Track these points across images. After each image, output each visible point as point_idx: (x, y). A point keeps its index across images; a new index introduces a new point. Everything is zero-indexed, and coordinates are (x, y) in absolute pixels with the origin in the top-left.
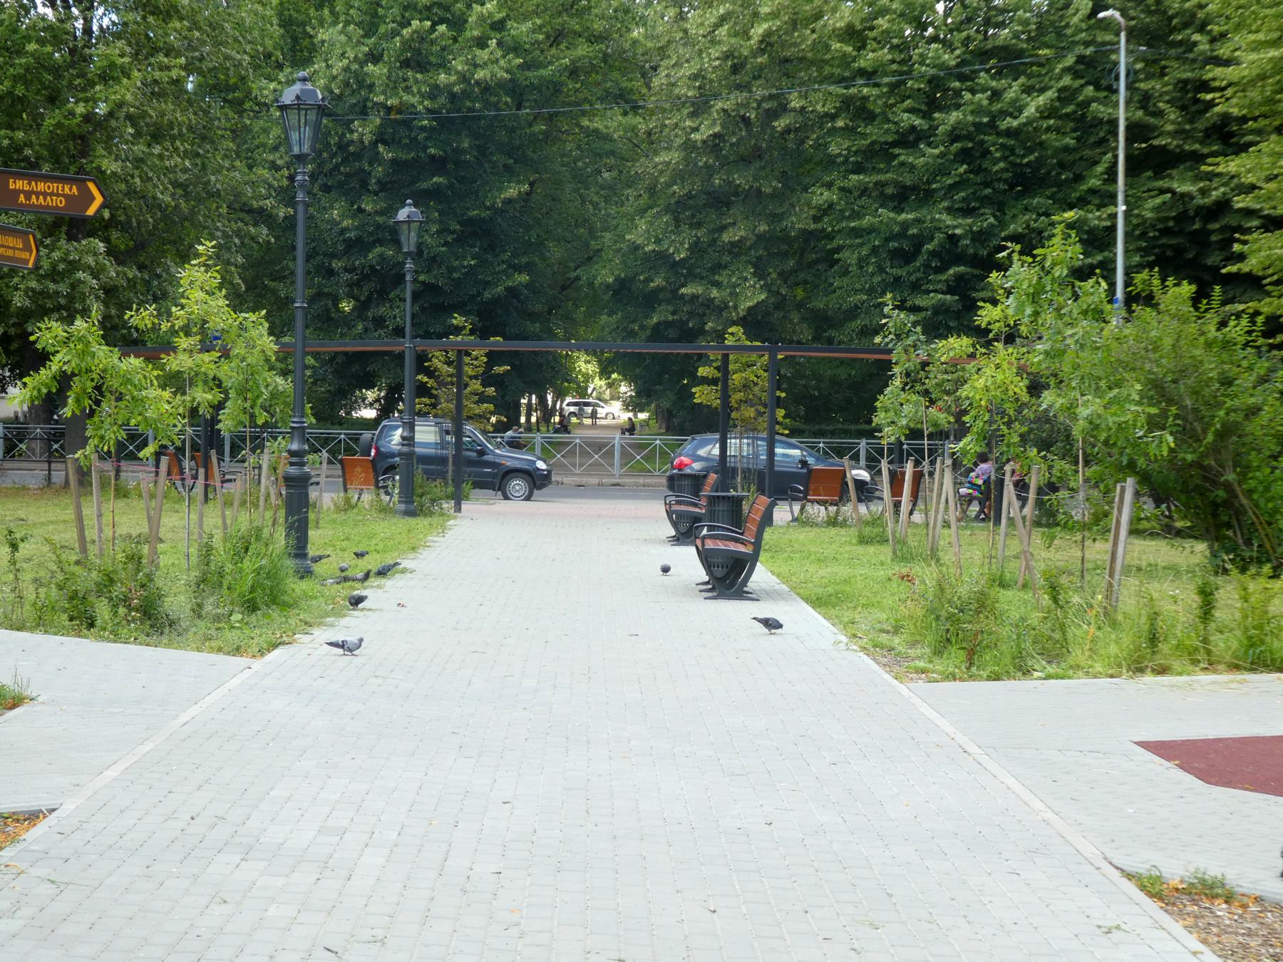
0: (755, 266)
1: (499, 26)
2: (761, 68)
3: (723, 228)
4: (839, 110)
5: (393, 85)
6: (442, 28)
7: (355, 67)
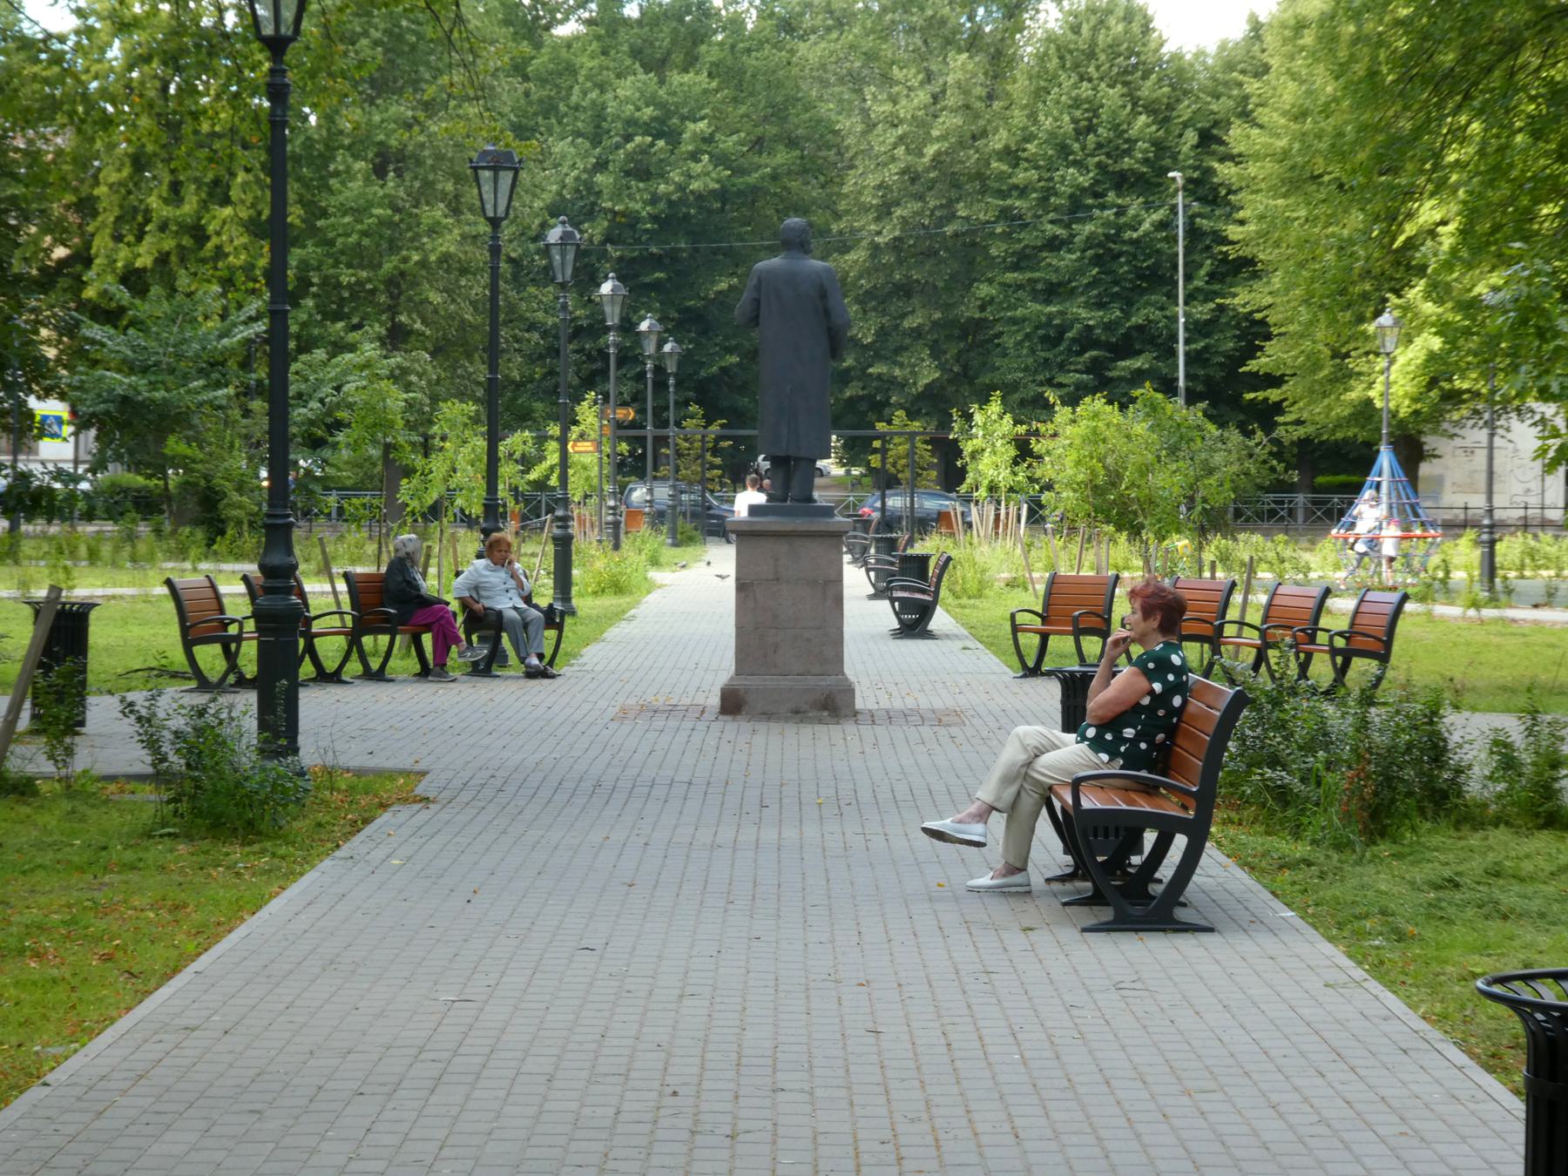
0: (931, 348)
1: (708, 140)
2: (934, 181)
3: (903, 316)
4: (998, 218)
5: (617, 195)
6: (661, 143)
7: (584, 176)
